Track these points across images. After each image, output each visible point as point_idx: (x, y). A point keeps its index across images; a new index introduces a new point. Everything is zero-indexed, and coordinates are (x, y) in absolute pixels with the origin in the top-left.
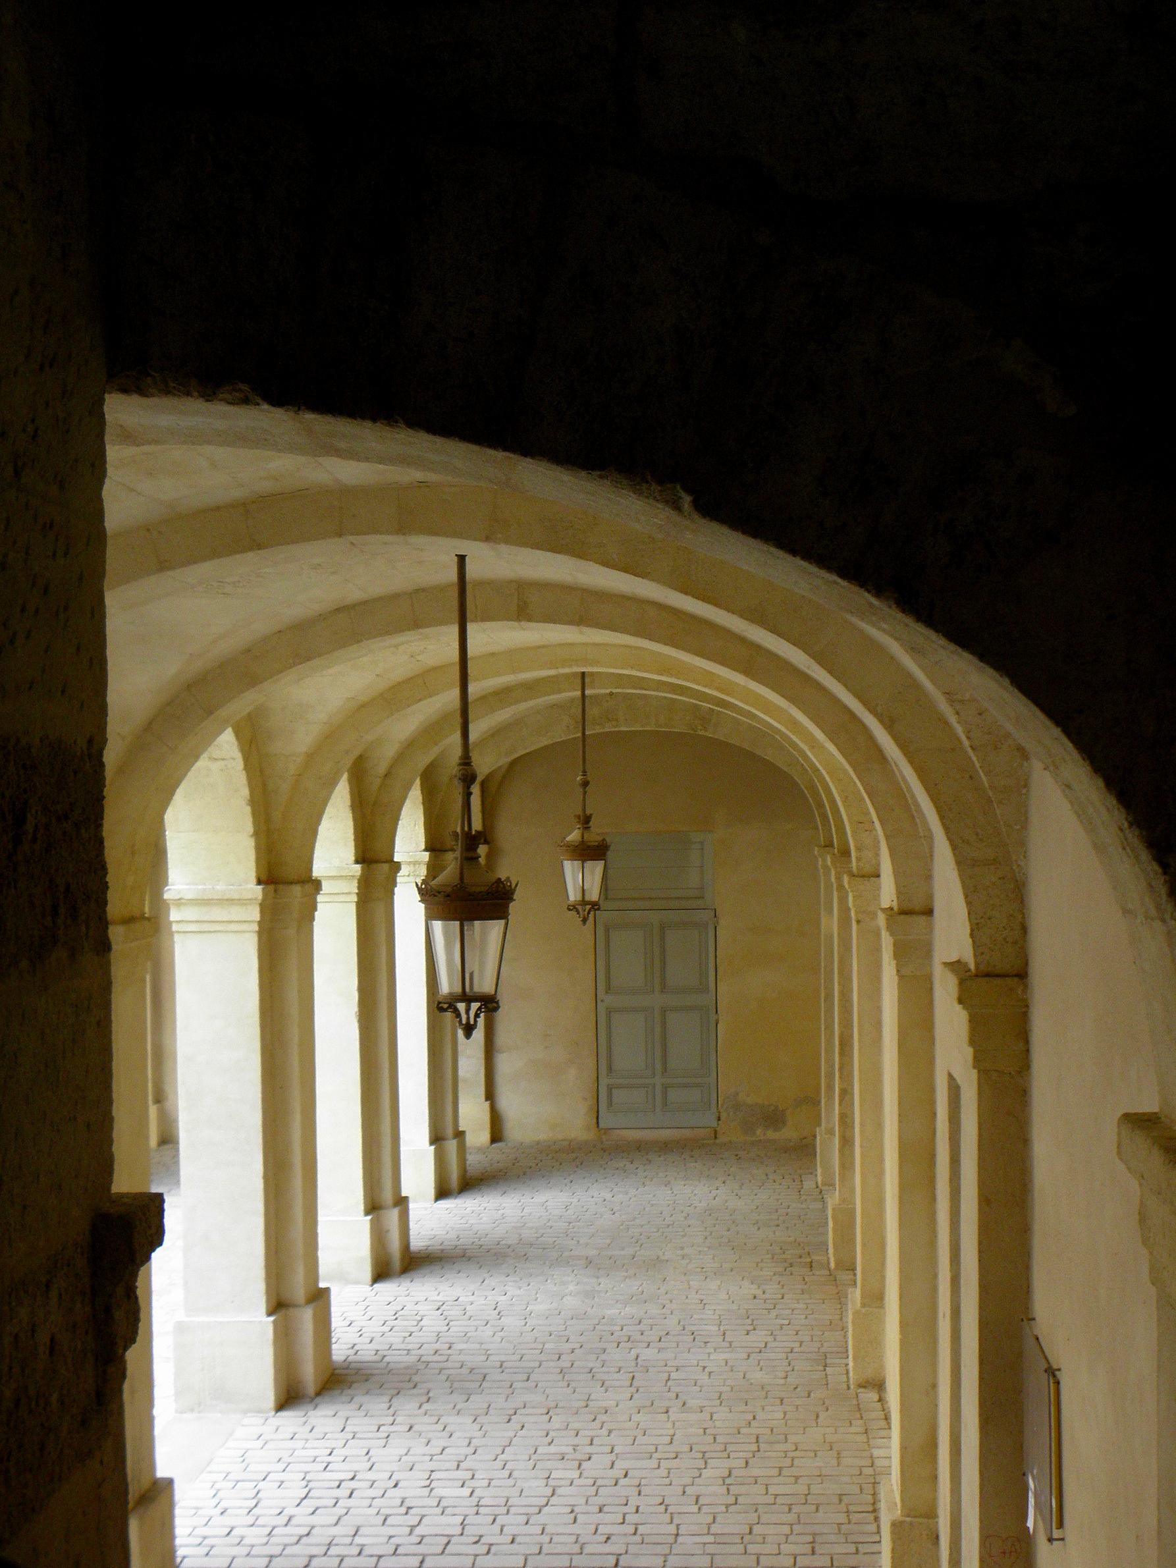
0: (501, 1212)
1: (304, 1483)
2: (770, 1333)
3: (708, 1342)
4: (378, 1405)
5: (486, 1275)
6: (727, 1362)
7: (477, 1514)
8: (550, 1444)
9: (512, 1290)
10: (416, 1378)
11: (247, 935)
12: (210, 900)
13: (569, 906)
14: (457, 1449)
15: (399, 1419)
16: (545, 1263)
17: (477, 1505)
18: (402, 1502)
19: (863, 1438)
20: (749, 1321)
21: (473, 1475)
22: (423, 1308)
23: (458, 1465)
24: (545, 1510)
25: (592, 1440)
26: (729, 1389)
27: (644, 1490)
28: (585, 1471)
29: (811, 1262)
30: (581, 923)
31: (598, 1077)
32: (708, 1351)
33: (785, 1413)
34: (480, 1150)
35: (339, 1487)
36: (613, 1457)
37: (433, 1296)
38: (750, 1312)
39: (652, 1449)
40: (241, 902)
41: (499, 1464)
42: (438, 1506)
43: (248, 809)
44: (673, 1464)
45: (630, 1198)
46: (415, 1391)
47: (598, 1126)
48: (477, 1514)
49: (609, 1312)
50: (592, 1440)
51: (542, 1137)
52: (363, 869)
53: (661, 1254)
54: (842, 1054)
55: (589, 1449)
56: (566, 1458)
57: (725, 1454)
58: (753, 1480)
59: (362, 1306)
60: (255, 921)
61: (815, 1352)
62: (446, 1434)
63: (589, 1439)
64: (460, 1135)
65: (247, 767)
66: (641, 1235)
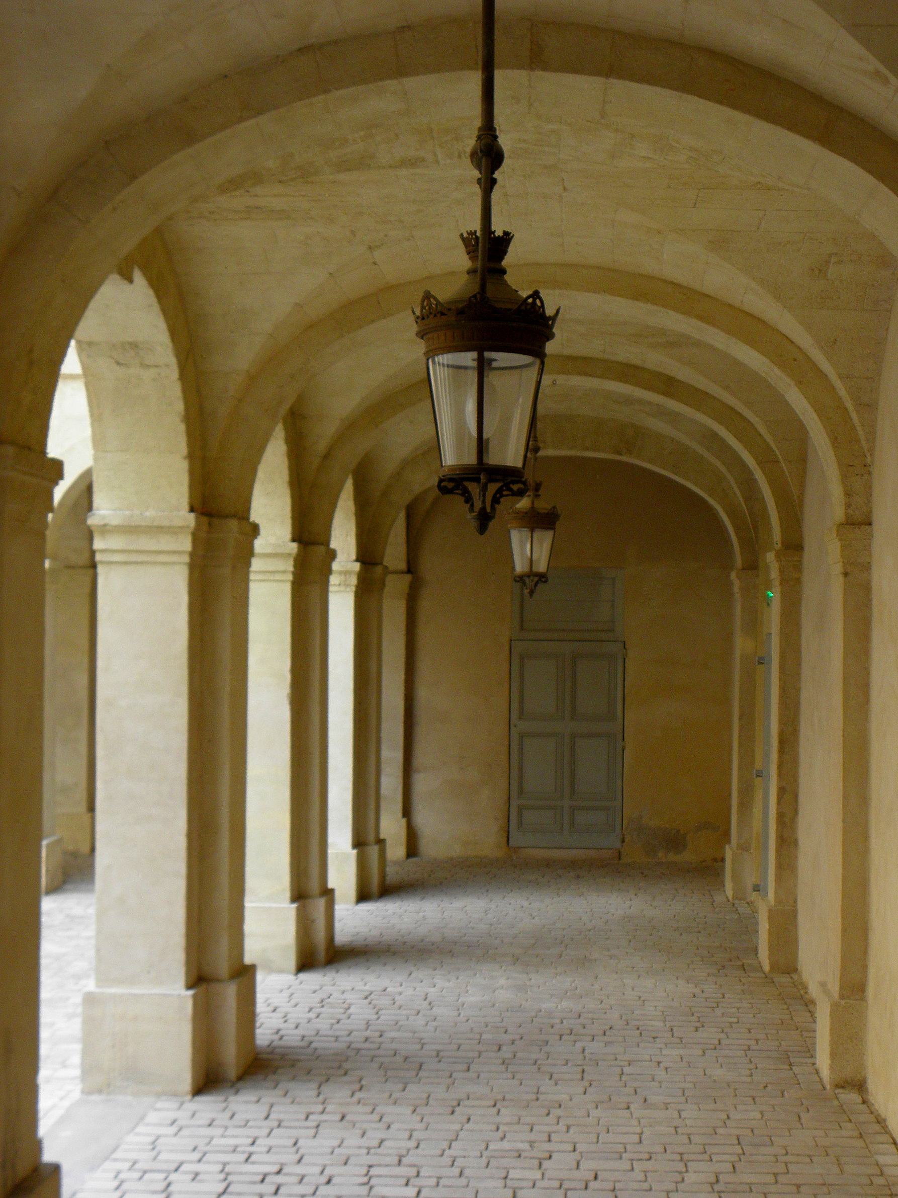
0: (421, 914)
1: (222, 1176)
2: (720, 1030)
3: (657, 1037)
4: (305, 1092)
5: (412, 968)
6: (682, 1058)
9: (440, 982)
10: (346, 1066)
14: (397, 1143)
15: (329, 1108)
19: (859, 1143)
20: (694, 1018)
22: (350, 997)
23: (400, 1161)
25: (549, 1136)
26: (691, 1085)
29: (743, 965)
32: (659, 1046)
33: (762, 1113)
34: (395, 863)
35: (262, 1181)
36: (576, 1156)
37: (360, 986)
38: (693, 1010)
39: (621, 1148)
41: (446, 1160)
43: (182, 427)
44: (649, 1165)
46: (345, 1078)
52: (299, 548)
54: (782, 751)
55: (547, 1146)
56: (522, 1156)
57: (706, 1157)
58: (747, 1188)
59: (286, 994)
61: (775, 1051)
63: (546, 1135)
64: (381, 842)
65: (183, 377)
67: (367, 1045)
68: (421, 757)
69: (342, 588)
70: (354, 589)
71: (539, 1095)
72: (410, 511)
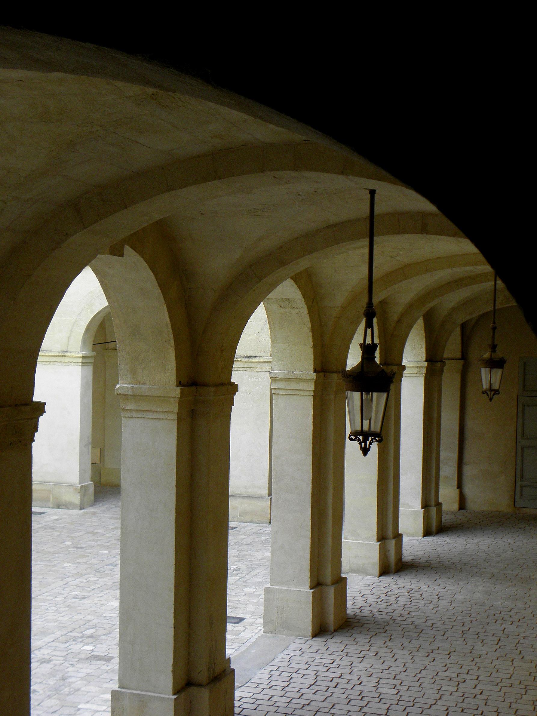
0: (455, 545)
1: (315, 677)
4: (363, 640)
5: (438, 577)
7: (397, 704)
8: (445, 671)
9: (449, 587)
11: (308, 397)
12: (291, 378)
13: (483, 391)
14: (397, 668)
15: (372, 648)
16: (470, 574)
17: (399, 700)
18: (361, 693)
21: (401, 683)
24: (433, 707)
27: (489, 703)
28: (532, 673)
30: (489, 400)
31: (515, 481)
37: (408, 586)
39: (499, 680)
40: (306, 380)
42: (378, 698)
45: (523, 544)
46: (384, 635)
47: (514, 506)
48: (397, 704)
49: (495, 603)
50: (468, 671)
51: (486, 508)
53: (532, 575)
55: (466, 676)
60: (311, 390)
62: (394, 659)
64: (439, 505)
66: (524, 564)
67: (401, 618)
68: (468, 456)
69: (418, 375)
70: (424, 375)
71: (472, 651)
72: (463, 326)
